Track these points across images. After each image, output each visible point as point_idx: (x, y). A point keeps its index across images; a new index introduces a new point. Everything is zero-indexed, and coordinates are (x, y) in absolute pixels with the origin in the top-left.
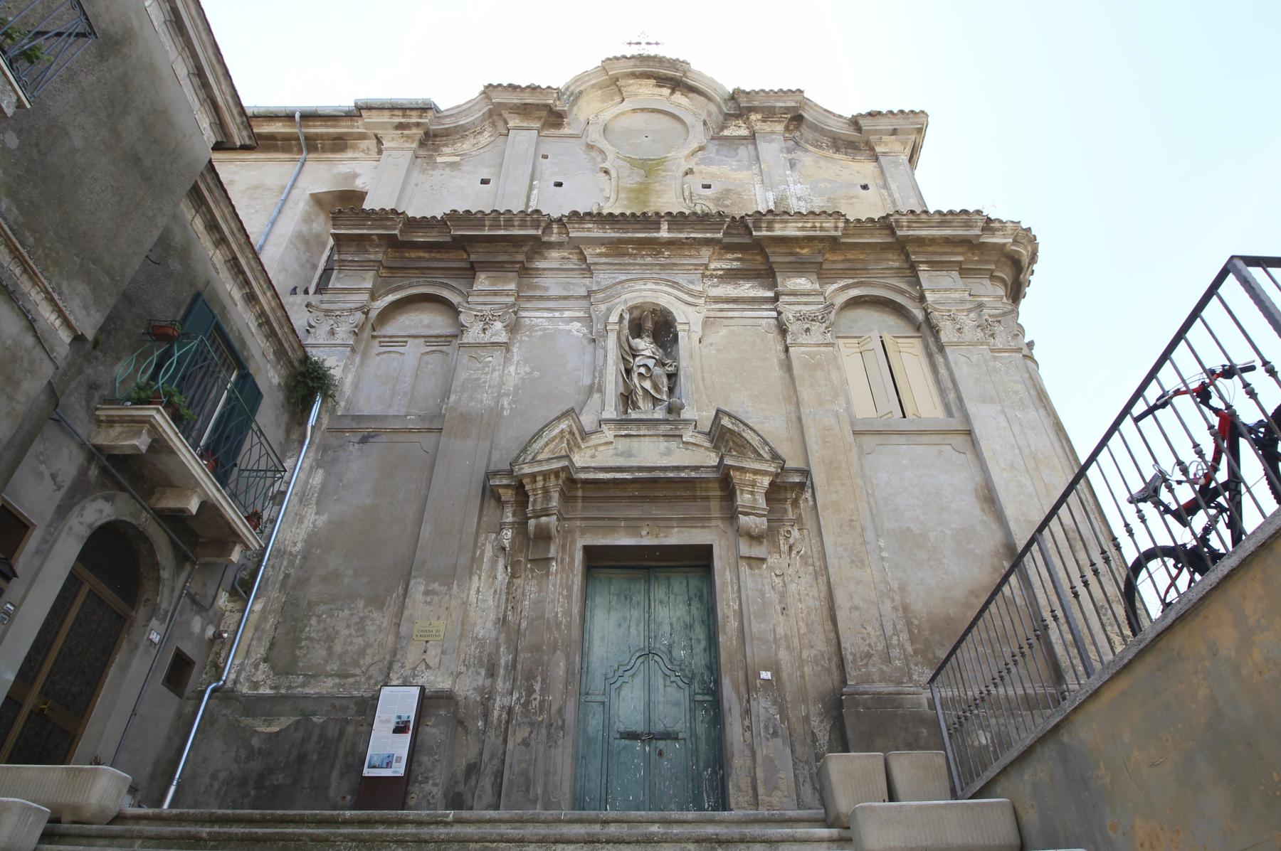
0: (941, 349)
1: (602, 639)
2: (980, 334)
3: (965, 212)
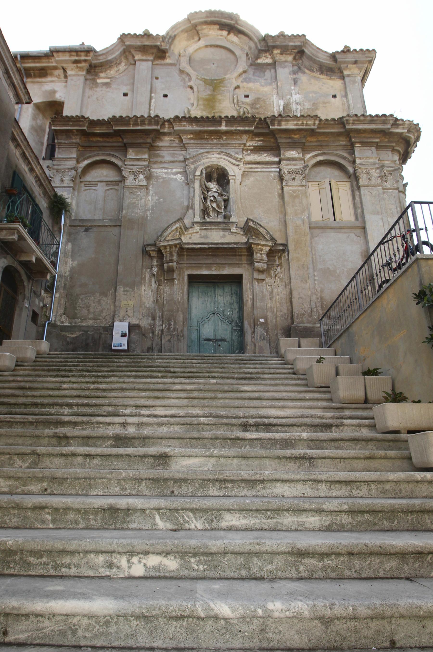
0: (359, 188)
1: (196, 308)
2: (379, 181)
3: (384, 115)
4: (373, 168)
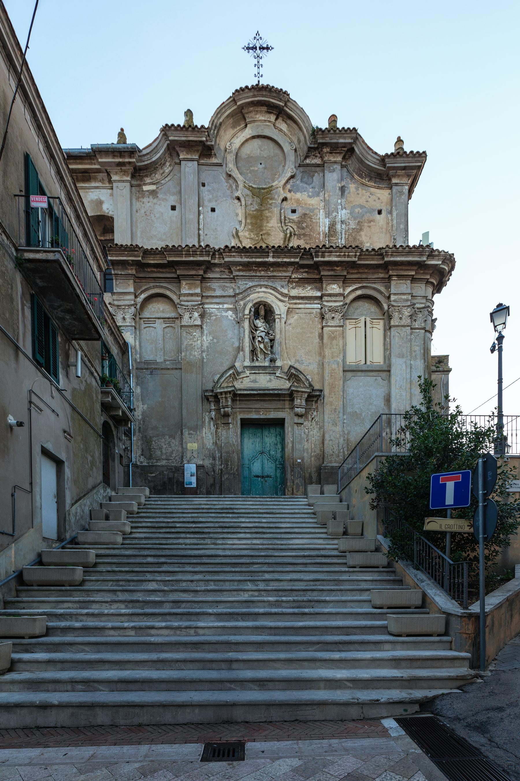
2: (409, 321)
4: (405, 306)
